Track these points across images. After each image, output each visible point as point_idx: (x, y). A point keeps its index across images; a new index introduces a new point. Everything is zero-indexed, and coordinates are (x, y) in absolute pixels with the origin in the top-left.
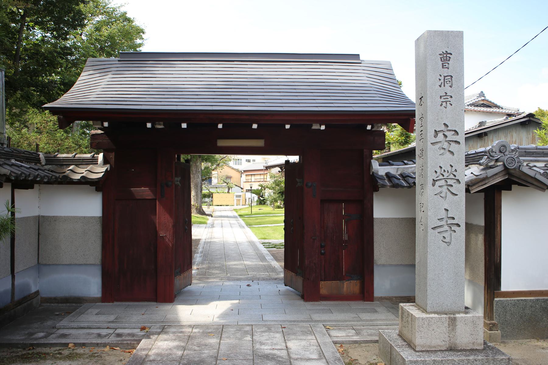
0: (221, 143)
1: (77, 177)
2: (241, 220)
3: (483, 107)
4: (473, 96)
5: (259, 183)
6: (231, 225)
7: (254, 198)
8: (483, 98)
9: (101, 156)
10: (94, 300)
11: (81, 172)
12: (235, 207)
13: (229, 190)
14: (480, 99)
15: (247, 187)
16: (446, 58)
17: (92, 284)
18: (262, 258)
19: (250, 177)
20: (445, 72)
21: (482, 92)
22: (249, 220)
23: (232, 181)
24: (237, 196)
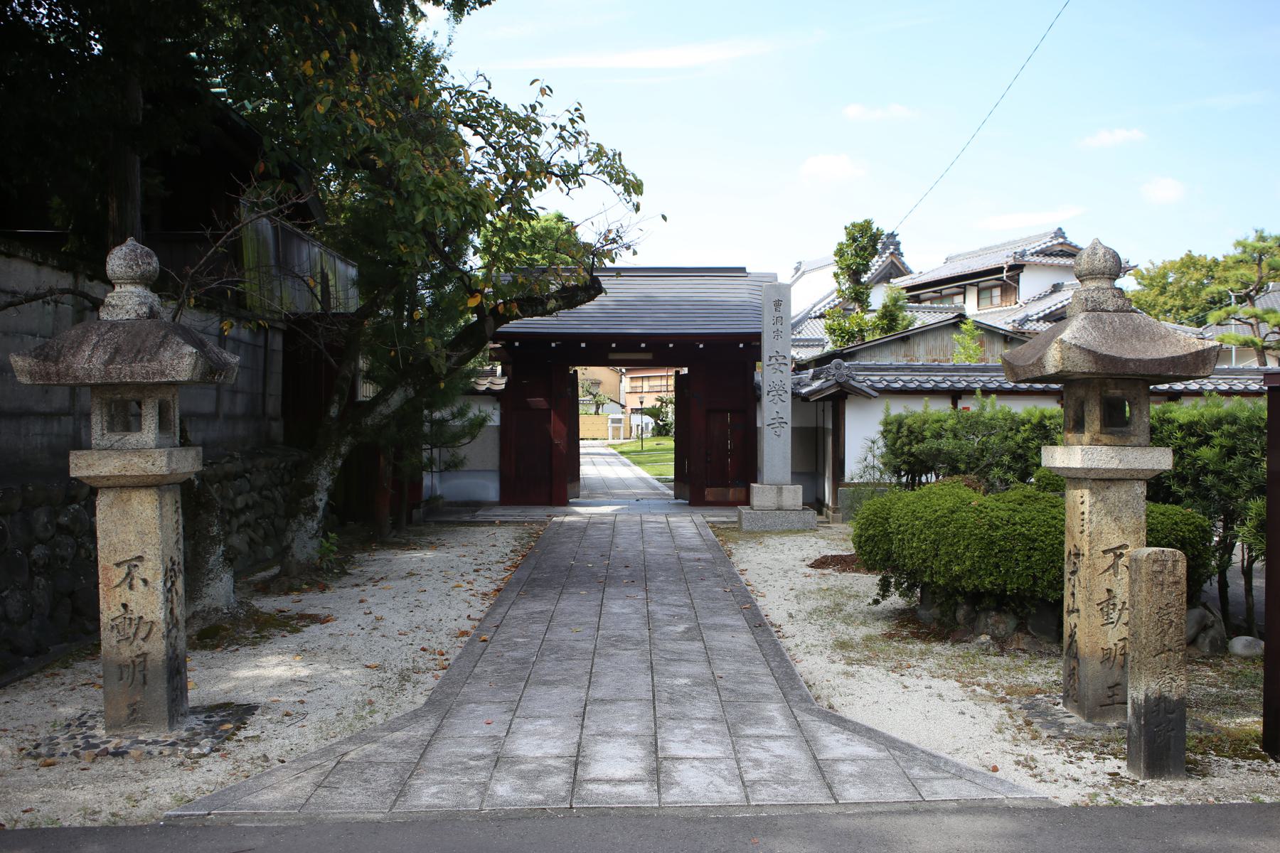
0: (612, 356)
1: (483, 388)
2: (623, 458)
3: (1062, 256)
4: (1045, 235)
5: (656, 395)
6: (608, 464)
7: (647, 424)
8: (1061, 240)
9: (499, 369)
10: (491, 505)
11: (484, 384)
12: (611, 441)
13: (598, 408)
14: (1055, 242)
15: (633, 402)
16: (778, 304)
17: (490, 489)
18: (655, 488)
19: (639, 384)
20: (777, 314)
21: (1060, 229)
22: (637, 457)
23: (600, 390)
24: (614, 421)
